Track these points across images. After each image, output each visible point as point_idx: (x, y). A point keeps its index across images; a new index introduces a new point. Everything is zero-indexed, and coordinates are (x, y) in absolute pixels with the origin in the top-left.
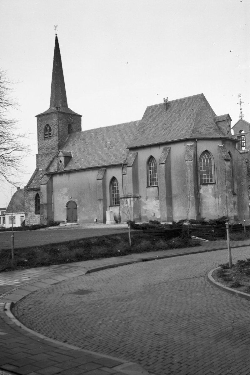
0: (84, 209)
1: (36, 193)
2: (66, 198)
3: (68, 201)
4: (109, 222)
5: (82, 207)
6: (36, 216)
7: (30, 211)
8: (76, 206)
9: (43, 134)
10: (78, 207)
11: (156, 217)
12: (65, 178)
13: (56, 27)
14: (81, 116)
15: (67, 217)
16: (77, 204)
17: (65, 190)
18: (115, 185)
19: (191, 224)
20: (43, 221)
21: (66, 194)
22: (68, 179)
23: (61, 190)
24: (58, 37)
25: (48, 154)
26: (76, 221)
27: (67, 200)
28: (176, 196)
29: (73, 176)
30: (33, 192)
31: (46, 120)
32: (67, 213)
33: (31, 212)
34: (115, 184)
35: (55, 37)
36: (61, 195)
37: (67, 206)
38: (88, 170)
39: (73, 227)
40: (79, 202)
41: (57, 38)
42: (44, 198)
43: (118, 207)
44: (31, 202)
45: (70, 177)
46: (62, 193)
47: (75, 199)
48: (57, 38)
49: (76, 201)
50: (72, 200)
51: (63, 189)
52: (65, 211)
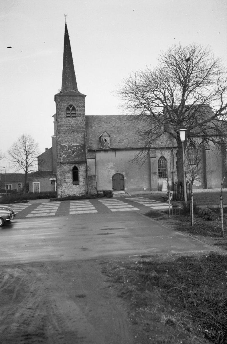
0: (132, 180)
1: (73, 166)
2: (111, 171)
3: (114, 173)
4: (165, 189)
5: (131, 179)
6: (74, 186)
7: (65, 182)
8: (123, 178)
9: (65, 113)
10: (125, 178)
11: (196, 185)
12: (110, 155)
13: (65, 16)
14: (85, 96)
15: (113, 187)
16: (124, 176)
17: (111, 165)
18: (161, 162)
19: (10, 220)
20: (92, 190)
21: (112, 168)
22: (115, 155)
23: (106, 164)
24: (67, 25)
25: (73, 131)
26: (123, 189)
27: (113, 172)
28: (212, 172)
29: (119, 154)
30: (69, 166)
31: (69, 100)
32: (113, 183)
33: (67, 183)
34: (161, 161)
35: (65, 25)
36: (106, 168)
37: (112, 178)
38: (136, 150)
39: (152, 194)
40: (127, 174)
41: (66, 26)
42: (92, 170)
43: (166, 179)
44: (66, 174)
45: (116, 154)
46: (107, 166)
47: (122, 172)
48: (66, 26)
49: (124, 173)
50: (118, 173)
51: (109, 163)
52: (112, 181)
